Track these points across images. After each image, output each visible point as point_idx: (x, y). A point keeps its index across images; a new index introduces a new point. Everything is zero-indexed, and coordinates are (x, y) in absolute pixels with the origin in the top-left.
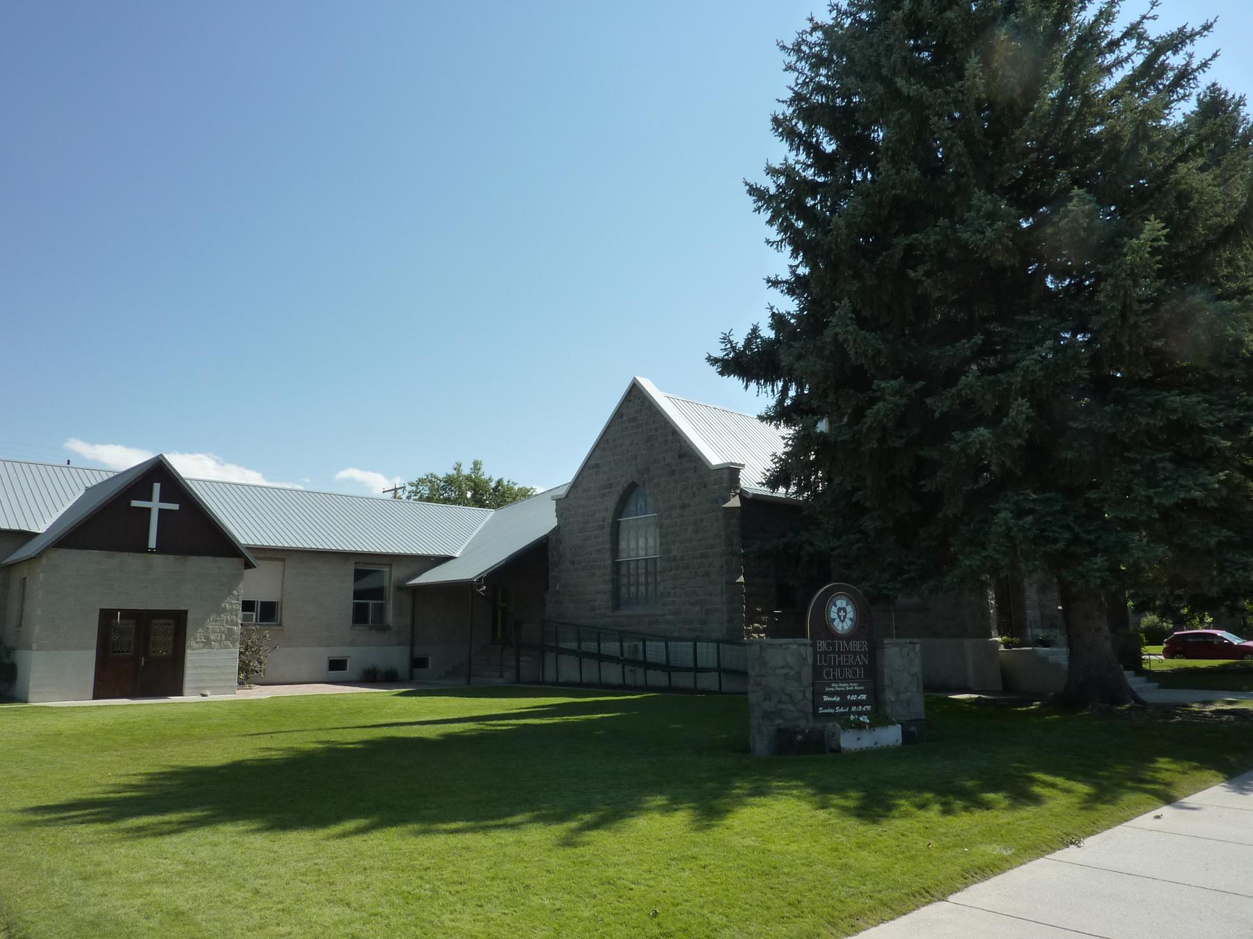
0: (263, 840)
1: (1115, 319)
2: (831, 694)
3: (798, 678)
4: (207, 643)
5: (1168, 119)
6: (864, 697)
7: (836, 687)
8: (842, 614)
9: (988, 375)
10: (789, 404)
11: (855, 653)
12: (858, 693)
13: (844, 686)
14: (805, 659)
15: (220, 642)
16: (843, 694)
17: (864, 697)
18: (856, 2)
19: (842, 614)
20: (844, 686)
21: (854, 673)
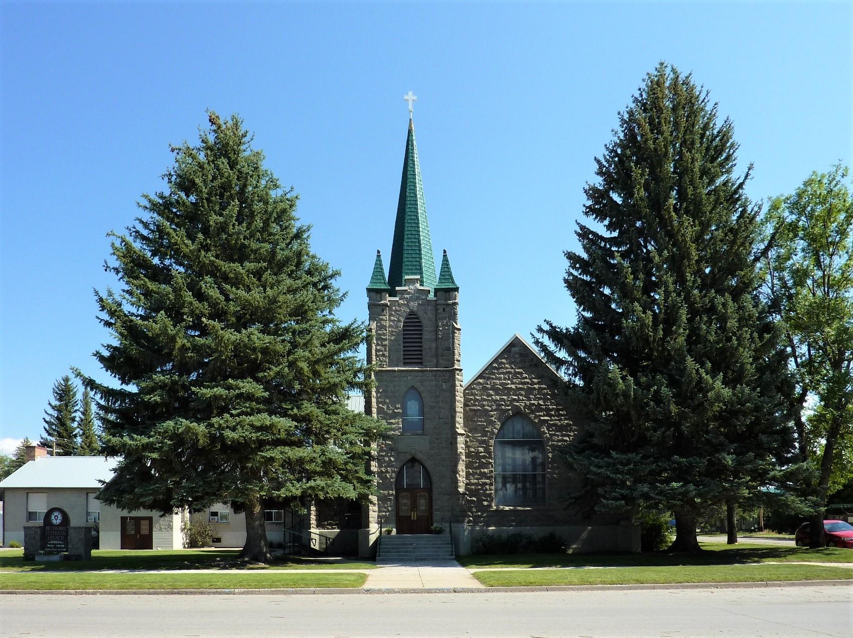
0: (102, 429)
1: (132, 479)
2: (50, 544)
3: (34, 538)
4: (161, 529)
5: (506, 487)
6: (63, 546)
7: (52, 542)
8: (56, 518)
9: (643, 536)
10: (726, 509)
11: (61, 531)
12: (61, 544)
13: (56, 542)
14: (37, 532)
15: (166, 529)
16: (55, 544)
17: (63, 546)
18: (849, 388)
19: (56, 518)
20: (56, 542)
21: (60, 538)
